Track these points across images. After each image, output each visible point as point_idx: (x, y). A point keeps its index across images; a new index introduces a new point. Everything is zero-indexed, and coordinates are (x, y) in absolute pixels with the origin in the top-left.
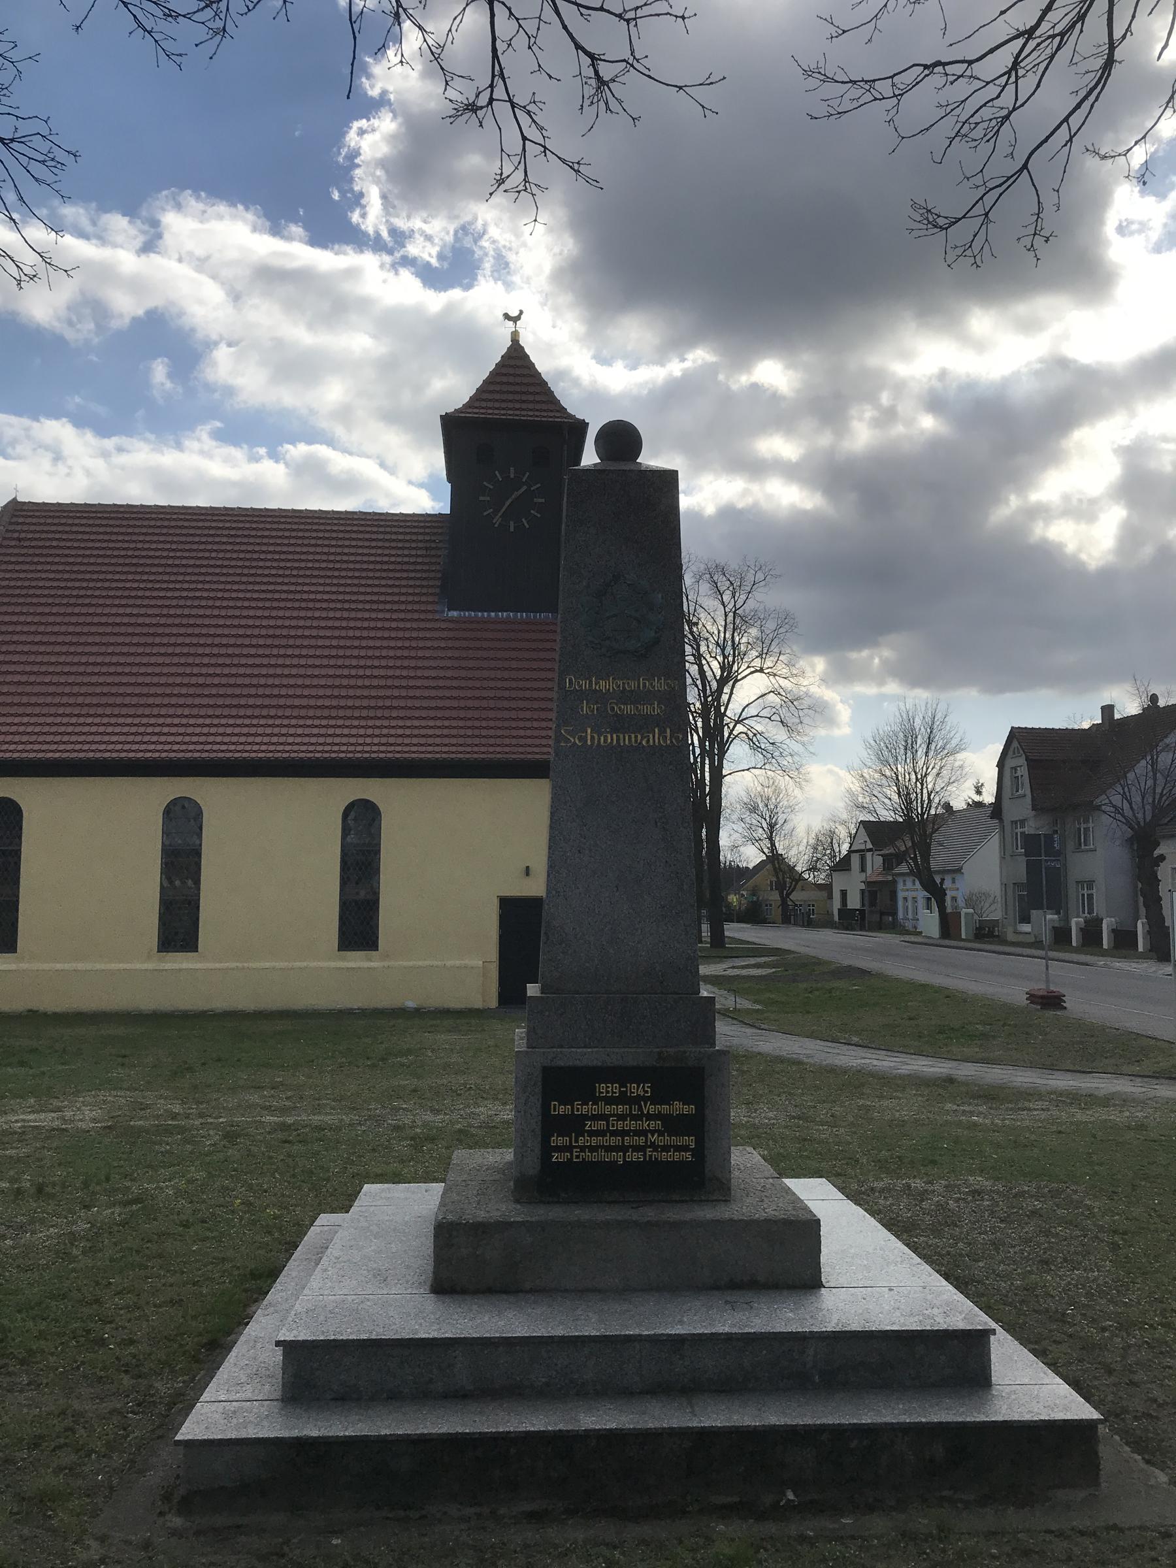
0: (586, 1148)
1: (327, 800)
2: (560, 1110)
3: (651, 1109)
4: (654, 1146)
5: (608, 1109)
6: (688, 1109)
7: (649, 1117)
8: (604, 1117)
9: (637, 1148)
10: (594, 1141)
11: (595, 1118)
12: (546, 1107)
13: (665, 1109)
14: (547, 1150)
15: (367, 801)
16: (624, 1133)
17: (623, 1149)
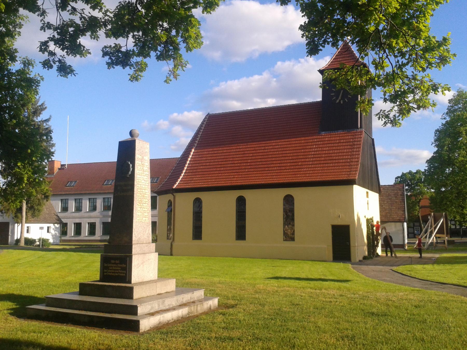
1: (234, 195)
2: (106, 265)
6: (125, 266)
10: (110, 271)
13: (121, 265)
14: (104, 272)
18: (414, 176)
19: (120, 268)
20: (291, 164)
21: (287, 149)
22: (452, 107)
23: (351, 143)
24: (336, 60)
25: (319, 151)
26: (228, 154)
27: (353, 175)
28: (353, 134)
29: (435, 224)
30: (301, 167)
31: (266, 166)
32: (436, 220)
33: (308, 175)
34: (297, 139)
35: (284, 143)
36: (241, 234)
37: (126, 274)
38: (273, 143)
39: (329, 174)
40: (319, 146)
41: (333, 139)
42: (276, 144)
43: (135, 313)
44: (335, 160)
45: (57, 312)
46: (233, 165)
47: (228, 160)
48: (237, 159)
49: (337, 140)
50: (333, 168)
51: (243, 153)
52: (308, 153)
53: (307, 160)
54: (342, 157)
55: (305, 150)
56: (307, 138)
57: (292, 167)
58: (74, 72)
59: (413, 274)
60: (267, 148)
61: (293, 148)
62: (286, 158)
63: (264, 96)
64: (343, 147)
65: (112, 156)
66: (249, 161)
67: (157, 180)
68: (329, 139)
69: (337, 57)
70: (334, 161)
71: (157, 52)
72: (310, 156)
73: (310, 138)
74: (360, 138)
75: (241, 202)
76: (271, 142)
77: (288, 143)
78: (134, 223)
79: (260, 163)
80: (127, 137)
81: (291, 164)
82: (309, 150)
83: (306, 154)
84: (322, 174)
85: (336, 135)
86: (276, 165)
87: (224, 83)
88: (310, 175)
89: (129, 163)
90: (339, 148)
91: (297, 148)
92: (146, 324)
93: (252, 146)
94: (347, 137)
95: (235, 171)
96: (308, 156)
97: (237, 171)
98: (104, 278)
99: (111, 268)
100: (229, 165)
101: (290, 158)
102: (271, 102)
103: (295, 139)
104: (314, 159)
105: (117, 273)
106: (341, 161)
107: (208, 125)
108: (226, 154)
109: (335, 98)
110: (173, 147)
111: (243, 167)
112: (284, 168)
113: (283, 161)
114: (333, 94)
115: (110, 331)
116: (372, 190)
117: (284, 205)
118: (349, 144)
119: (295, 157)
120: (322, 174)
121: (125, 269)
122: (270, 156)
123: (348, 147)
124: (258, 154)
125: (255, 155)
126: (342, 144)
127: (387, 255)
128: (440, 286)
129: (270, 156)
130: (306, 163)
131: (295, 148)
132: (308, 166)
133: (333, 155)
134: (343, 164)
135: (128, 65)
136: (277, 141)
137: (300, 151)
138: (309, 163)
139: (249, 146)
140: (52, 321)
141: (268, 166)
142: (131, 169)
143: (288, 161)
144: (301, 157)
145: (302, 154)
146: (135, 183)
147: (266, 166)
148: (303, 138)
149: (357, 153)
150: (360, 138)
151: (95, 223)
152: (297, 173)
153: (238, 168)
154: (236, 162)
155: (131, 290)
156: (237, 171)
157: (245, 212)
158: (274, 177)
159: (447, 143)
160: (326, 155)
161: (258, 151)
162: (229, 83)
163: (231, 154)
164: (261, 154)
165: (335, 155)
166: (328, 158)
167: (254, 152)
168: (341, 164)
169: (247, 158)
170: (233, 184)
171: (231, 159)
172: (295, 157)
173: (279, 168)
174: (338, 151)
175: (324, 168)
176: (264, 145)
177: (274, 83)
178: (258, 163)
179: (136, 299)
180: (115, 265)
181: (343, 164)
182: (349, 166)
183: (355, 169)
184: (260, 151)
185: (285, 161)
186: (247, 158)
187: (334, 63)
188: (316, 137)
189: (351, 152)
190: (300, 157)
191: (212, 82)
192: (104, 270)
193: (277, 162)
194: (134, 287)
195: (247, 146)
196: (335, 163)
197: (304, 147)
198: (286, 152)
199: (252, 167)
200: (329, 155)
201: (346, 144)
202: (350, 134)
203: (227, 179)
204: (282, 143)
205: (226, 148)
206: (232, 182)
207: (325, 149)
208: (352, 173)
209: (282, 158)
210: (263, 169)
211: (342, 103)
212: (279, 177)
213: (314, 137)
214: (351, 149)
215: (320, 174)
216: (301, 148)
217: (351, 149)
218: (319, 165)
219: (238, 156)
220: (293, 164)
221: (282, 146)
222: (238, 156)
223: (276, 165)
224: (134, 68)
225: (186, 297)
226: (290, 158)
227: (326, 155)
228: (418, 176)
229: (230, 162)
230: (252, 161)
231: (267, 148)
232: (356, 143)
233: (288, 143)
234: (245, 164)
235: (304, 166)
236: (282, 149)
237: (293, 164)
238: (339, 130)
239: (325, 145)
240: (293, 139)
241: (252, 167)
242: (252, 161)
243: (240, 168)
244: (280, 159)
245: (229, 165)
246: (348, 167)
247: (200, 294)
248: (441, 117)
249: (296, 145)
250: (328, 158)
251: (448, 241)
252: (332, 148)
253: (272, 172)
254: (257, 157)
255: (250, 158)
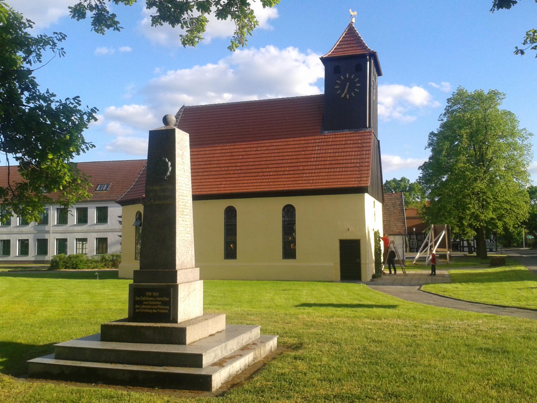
0: (144, 309)
3: (159, 299)
4: (160, 309)
5: (148, 299)
6: (167, 299)
7: (158, 301)
8: (148, 301)
9: (156, 309)
10: (146, 307)
11: (146, 301)
12: (134, 298)
13: (162, 299)
14: (135, 309)
15: (292, 206)
16: (152, 305)
17: (152, 309)
18: (398, 184)
19: (160, 303)
20: (291, 169)
21: (285, 150)
22: (450, 107)
23: (360, 145)
24: (341, 47)
25: (323, 153)
26: (211, 155)
27: (365, 182)
28: (361, 134)
29: (435, 238)
30: (303, 172)
31: (260, 170)
32: (437, 233)
33: (311, 181)
34: (296, 139)
35: (280, 144)
36: (289, 252)
37: (169, 310)
38: (267, 143)
39: (336, 180)
40: (322, 148)
41: (339, 139)
42: (270, 144)
43: (199, 365)
44: (343, 164)
45: (72, 367)
46: (219, 169)
47: (212, 162)
48: (223, 162)
49: (342, 141)
50: (340, 173)
51: (230, 154)
52: (310, 156)
53: (309, 163)
54: (350, 161)
55: (306, 152)
56: (307, 138)
57: (292, 172)
58: (118, 25)
59: (446, 294)
60: (259, 149)
61: (291, 150)
62: (284, 161)
63: (220, 90)
64: (351, 150)
65: (139, 150)
66: (239, 164)
67: (107, 187)
68: (334, 139)
69: (341, 43)
70: (341, 165)
71: (219, 6)
72: (312, 160)
73: (311, 138)
74: (370, 139)
75: (289, 212)
76: (264, 142)
77: (285, 143)
78: (177, 241)
79: (253, 167)
80: (160, 126)
81: (291, 169)
82: (311, 152)
83: (308, 156)
84: (328, 181)
85: (342, 136)
86: (272, 170)
87: (173, 72)
88: (314, 181)
89: (167, 160)
90: (346, 150)
91: (296, 150)
92: (218, 379)
93: (242, 146)
94: (355, 138)
95: (222, 176)
96: (310, 160)
97: (224, 176)
98: (134, 316)
99: (144, 303)
100: (214, 169)
101: (289, 161)
102: (227, 98)
103: (293, 139)
104: (317, 163)
105: (156, 309)
106: (349, 165)
107: (184, 120)
108: (209, 156)
109: (339, 91)
110: (108, 148)
111: (232, 172)
112: (282, 173)
113: (281, 165)
114: (338, 87)
115: (168, 391)
116: (378, 199)
117: (283, 217)
118: (357, 145)
119: (294, 161)
120: (328, 181)
121: (168, 303)
122: (264, 159)
123: (356, 149)
124: (249, 156)
125: (246, 157)
126: (348, 146)
127: (390, 272)
128: (502, 308)
129: (264, 159)
130: (308, 167)
131: (294, 150)
132: (311, 171)
133: (339, 158)
134: (352, 169)
135: (179, 21)
136: (271, 141)
137: (300, 153)
138: (311, 167)
139: (237, 147)
140: (71, 381)
141: (262, 170)
142: (170, 169)
143: (286, 165)
144: (302, 160)
145: (303, 156)
146: (177, 188)
147: (260, 170)
148: (303, 138)
149: (367, 156)
150: (370, 139)
151: (28, 240)
152: (299, 179)
153: (225, 172)
154: (222, 165)
155: (182, 331)
156: (224, 176)
157: (236, 225)
158: (271, 183)
159: (446, 147)
160: (331, 158)
161: (249, 153)
162: (179, 72)
163: (216, 155)
164: (253, 156)
165: (342, 158)
166: (333, 162)
167: (244, 153)
168: (349, 169)
169: (236, 161)
170: (221, 192)
171: (216, 162)
172: (294, 161)
173: (276, 173)
174: (345, 154)
175: (329, 174)
176: (255, 146)
177: (230, 74)
178: (250, 167)
179: (189, 344)
180: (152, 299)
181: (352, 169)
182: (359, 171)
183: (366, 175)
184: (252, 153)
185: (283, 165)
186: (236, 161)
187: (338, 50)
188: (318, 137)
189: (360, 155)
190: (300, 160)
191: (157, 70)
192: (134, 305)
193: (273, 166)
194: (187, 328)
195: (234, 147)
196: (342, 168)
197: (305, 149)
198: (283, 154)
199: (243, 171)
200: (334, 158)
201: (354, 146)
202: (358, 135)
203: (213, 186)
204: (278, 144)
205: (209, 149)
206: (219, 189)
207: (329, 151)
208: (362, 179)
209: (279, 162)
210: (256, 174)
211: (348, 97)
212: (276, 183)
213: (316, 137)
214: (360, 151)
215: (325, 181)
216: (301, 149)
217: (360, 151)
218: (324, 170)
219: (224, 158)
220: (293, 168)
221: (278, 147)
222: (224, 158)
223: (272, 170)
224: (187, 27)
225: (245, 338)
226: (289, 161)
227: (331, 158)
228: (402, 183)
229: (215, 166)
230: (242, 164)
231: (259, 149)
232: (365, 145)
233: (285, 143)
234: (233, 168)
235: (305, 171)
236: (279, 151)
237: (293, 168)
238: (345, 129)
239: (330, 147)
240: (291, 139)
241: (243, 171)
242: (242, 164)
243: (228, 172)
244: (276, 162)
245: (214, 169)
246: (357, 172)
247: (255, 333)
248: (438, 118)
249: (294, 146)
250: (333, 162)
251: (450, 257)
252: (337, 150)
253: (268, 177)
254: (248, 160)
255: (240, 161)
